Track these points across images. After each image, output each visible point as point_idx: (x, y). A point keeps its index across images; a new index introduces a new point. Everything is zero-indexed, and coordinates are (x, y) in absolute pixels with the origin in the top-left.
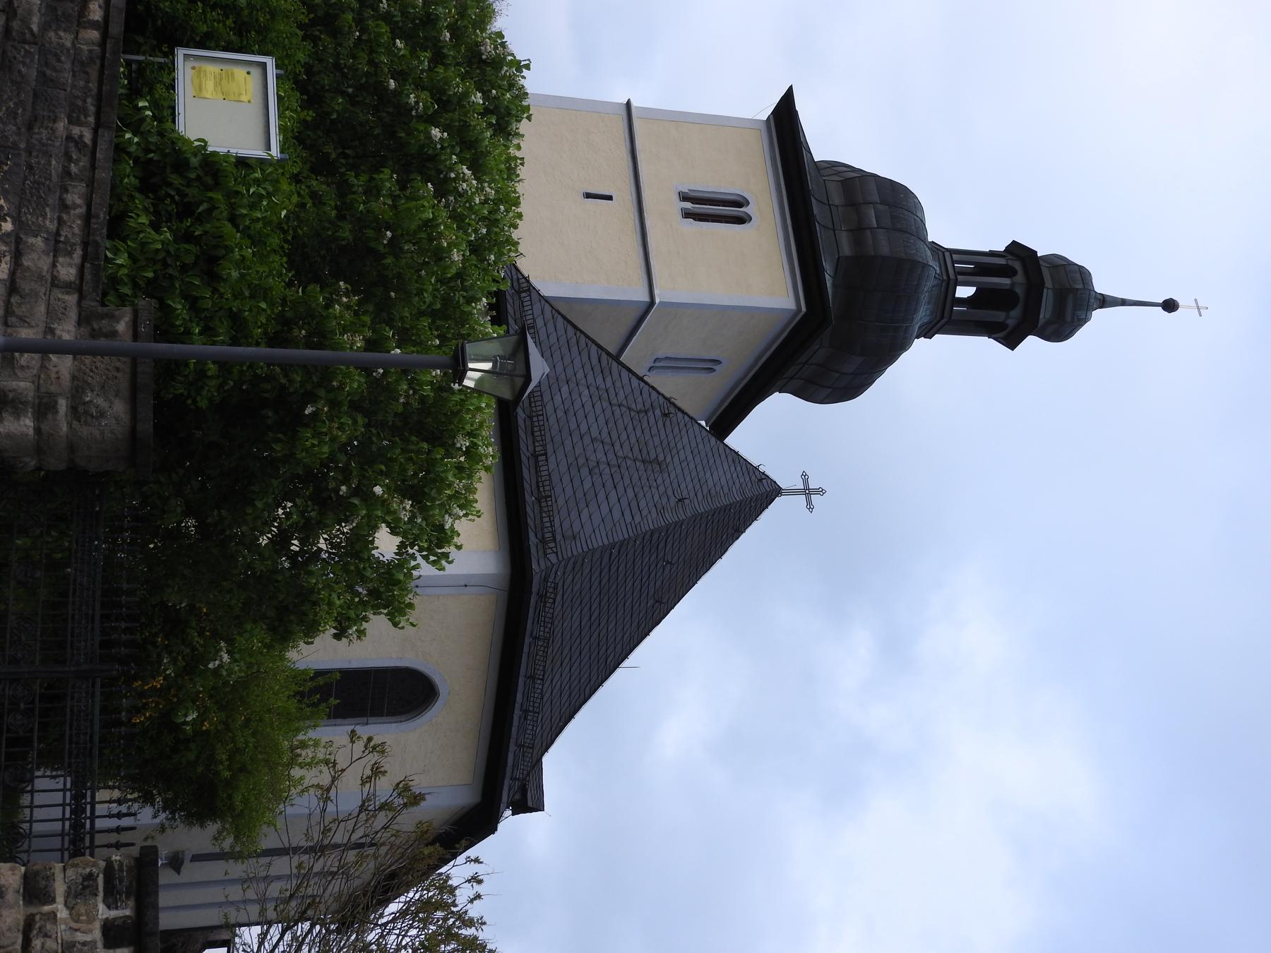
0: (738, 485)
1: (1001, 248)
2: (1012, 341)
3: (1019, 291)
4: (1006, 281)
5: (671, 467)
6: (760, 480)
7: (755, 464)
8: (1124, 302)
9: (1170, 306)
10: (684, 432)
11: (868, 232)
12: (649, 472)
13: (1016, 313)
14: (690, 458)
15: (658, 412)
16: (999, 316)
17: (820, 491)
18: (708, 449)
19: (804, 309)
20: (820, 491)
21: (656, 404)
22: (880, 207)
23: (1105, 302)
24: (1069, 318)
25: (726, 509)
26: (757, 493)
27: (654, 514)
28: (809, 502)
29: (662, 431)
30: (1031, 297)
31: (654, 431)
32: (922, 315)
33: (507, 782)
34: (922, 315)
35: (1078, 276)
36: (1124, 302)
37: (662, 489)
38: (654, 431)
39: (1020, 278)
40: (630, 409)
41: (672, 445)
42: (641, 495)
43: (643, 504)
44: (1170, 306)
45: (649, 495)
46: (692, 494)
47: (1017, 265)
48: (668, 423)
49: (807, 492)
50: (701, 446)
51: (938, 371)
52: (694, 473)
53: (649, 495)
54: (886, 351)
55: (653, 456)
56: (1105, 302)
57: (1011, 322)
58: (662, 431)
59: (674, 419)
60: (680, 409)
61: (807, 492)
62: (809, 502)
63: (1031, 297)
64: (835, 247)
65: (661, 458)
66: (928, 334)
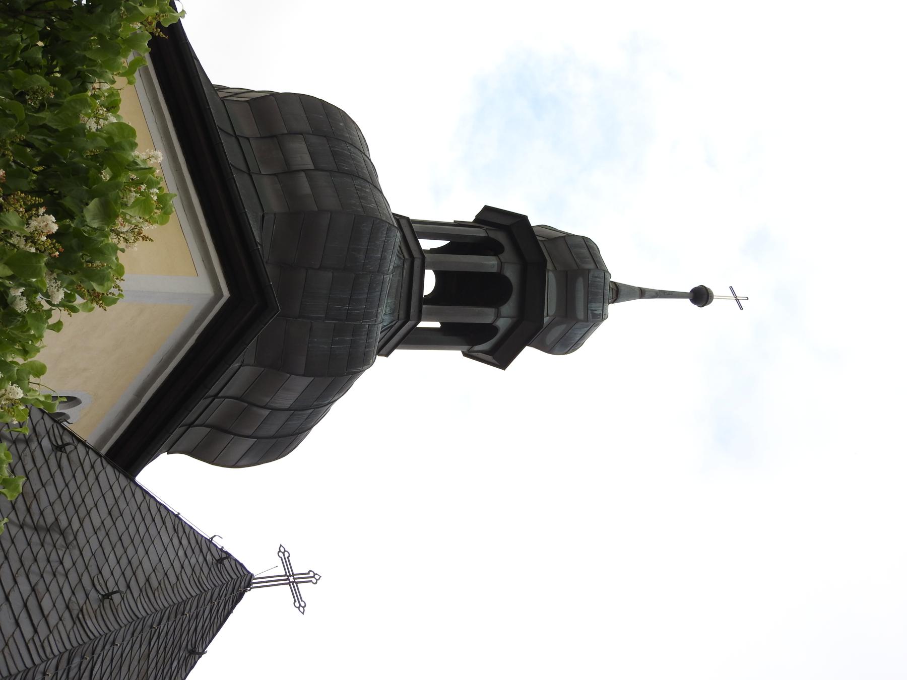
0: (188, 570)
1: (470, 218)
2: (501, 358)
3: (511, 273)
4: (489, 263)
5: (82, 540)
6: (220, 561)
7: (208, 534)
8: (642, 293)
9: (701, 296)
10: (92, 478)
11: (303, 174)
12: (49, 548)
13: (509, 308)
14: (108, 523)
15: (46, 443)
16: (485, 315)
17: (311, 577)
18: (134, 508)
19: (226, 294)
20: (311, 577)
21: (40, 429)
22: (314, 139)
23: (619, 293)
24: (581, 315)
25: (178, 609)
26: (222, 583)
27: (68, 623)
28: (297, 597)
29: (58, 476)
30: (519, 288)
31: (45, 475)
32: (384, 315)
33: (170, 185)
34: (384, 315)
35: (585, 251)
36: (642, 293)
37: (73, 577)
38: (45, 475)
39: (508, 254)
40: (36, 528)
41: (77, 499)
42: (41, 588)
43: (47, 604)
44: (701, 296)
45: (54, 589)
46: (123, 587)
47: (500, 237)
48: (64, 462)
49: (292, 579)
50: (122, 504)
51: (409, 400)
52: (119, 550)
53: (54, 589)
54: (337, 371)
55: (50, 519)
56: (619, 293)
57: (503, 324)
58: (58, 476)
59: (73, 456)
60: (79, 440)
61: (292, 579)
62: (297, 597)
63: (519, 288)
64: (261, 203)
65: (64, 523)
66: (385, 350)
